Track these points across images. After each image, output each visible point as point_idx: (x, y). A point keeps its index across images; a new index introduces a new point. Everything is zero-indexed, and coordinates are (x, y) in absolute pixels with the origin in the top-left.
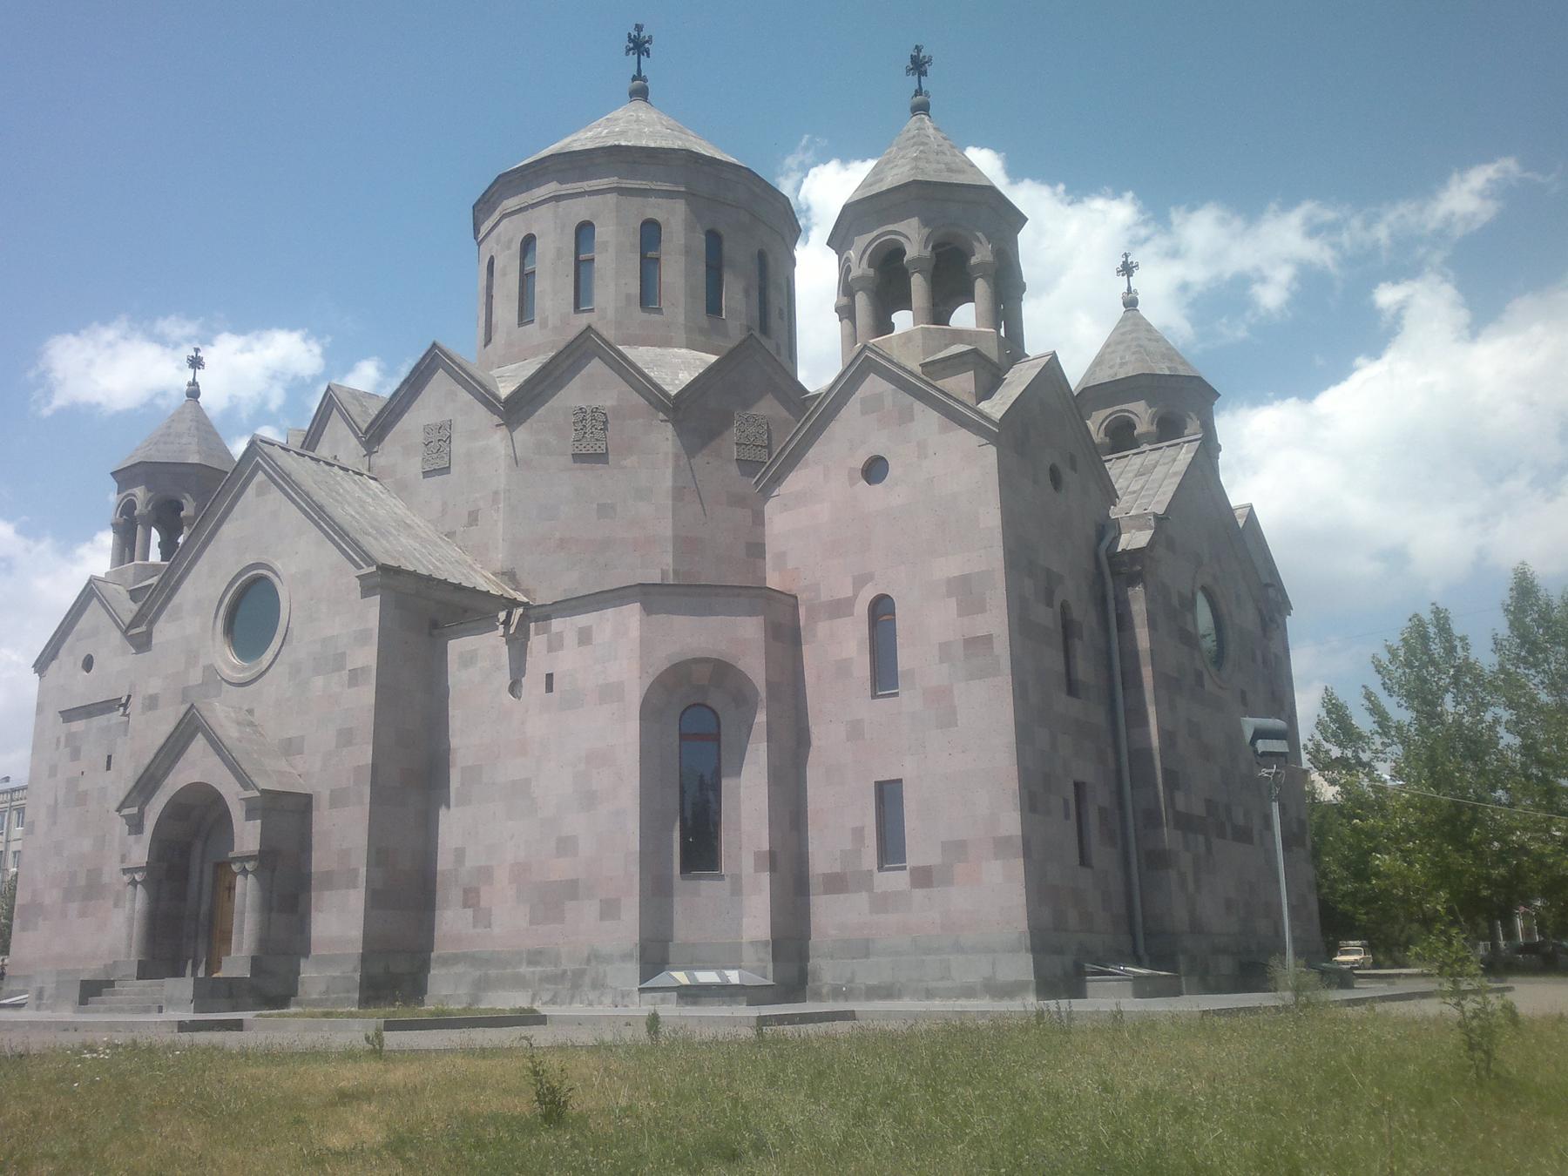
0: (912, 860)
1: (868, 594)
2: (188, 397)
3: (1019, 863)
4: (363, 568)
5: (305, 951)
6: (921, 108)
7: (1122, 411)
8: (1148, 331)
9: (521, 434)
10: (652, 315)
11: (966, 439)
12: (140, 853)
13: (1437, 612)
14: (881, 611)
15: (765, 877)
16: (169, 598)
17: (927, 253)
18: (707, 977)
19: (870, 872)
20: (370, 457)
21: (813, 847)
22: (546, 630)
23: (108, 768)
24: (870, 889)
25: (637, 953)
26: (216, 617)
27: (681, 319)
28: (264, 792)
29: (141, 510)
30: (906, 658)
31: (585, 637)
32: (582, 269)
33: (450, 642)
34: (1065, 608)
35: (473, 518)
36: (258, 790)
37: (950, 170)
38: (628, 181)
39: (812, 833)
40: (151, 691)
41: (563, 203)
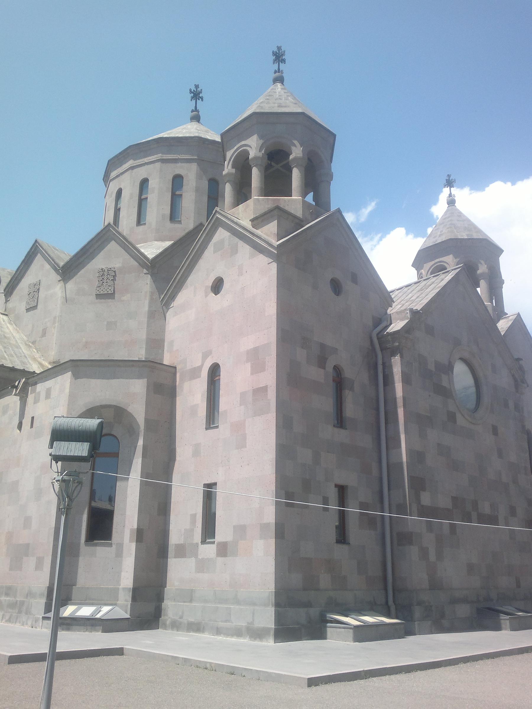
0: (219, 537)
6: (279, 79)
7: (441, 262)
8: (458, 216)
9: (70, 285)
15: (133, 546)
19: (197, 544)
20: (6, 303)
24: (196, 555)
34: (337, 369)
35: (44, 333)
38: (167, 155)
41: (135, 170)
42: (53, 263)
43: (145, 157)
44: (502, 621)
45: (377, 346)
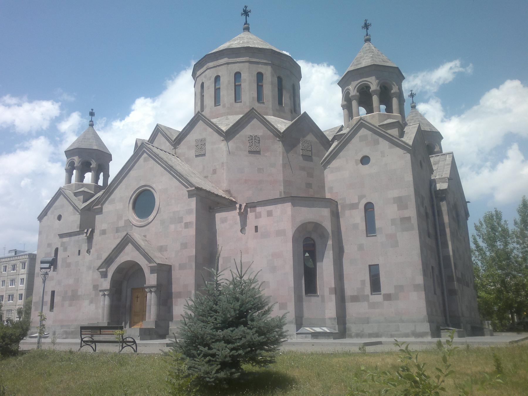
1: (364, 202)
2: (90, 126)
3: (423, 293)
4: (189, 188)
5: (171, 319)
6: (368, 40)
9: (231, 143)
10: (261, 104)
11: (399, 151)
12: (106, 284)
13: (496, 211)
14: (369, 208)
15: (333, 297)
16: (109, 196)
17: (378, 88)
18: (318, 330)
21: (346, 287)
22: (255, 211)
23: (79, 254)
25: (294, 321)
26: (129, 203)
27: (271, 106)
28: (158, 264)
29: (77, 165)
30: (378, 224)
31: (270, 214)
32: (237, 88)
33: (216, 214)
34: (425, 206)
35: (215, 172)
36: (156, 264)
37: (384, 61)
39: (346, 282)
40: (103, 228)
42: (217, 129)
43: (236, 57)
44: (485, 332)
45: (434, 197)
